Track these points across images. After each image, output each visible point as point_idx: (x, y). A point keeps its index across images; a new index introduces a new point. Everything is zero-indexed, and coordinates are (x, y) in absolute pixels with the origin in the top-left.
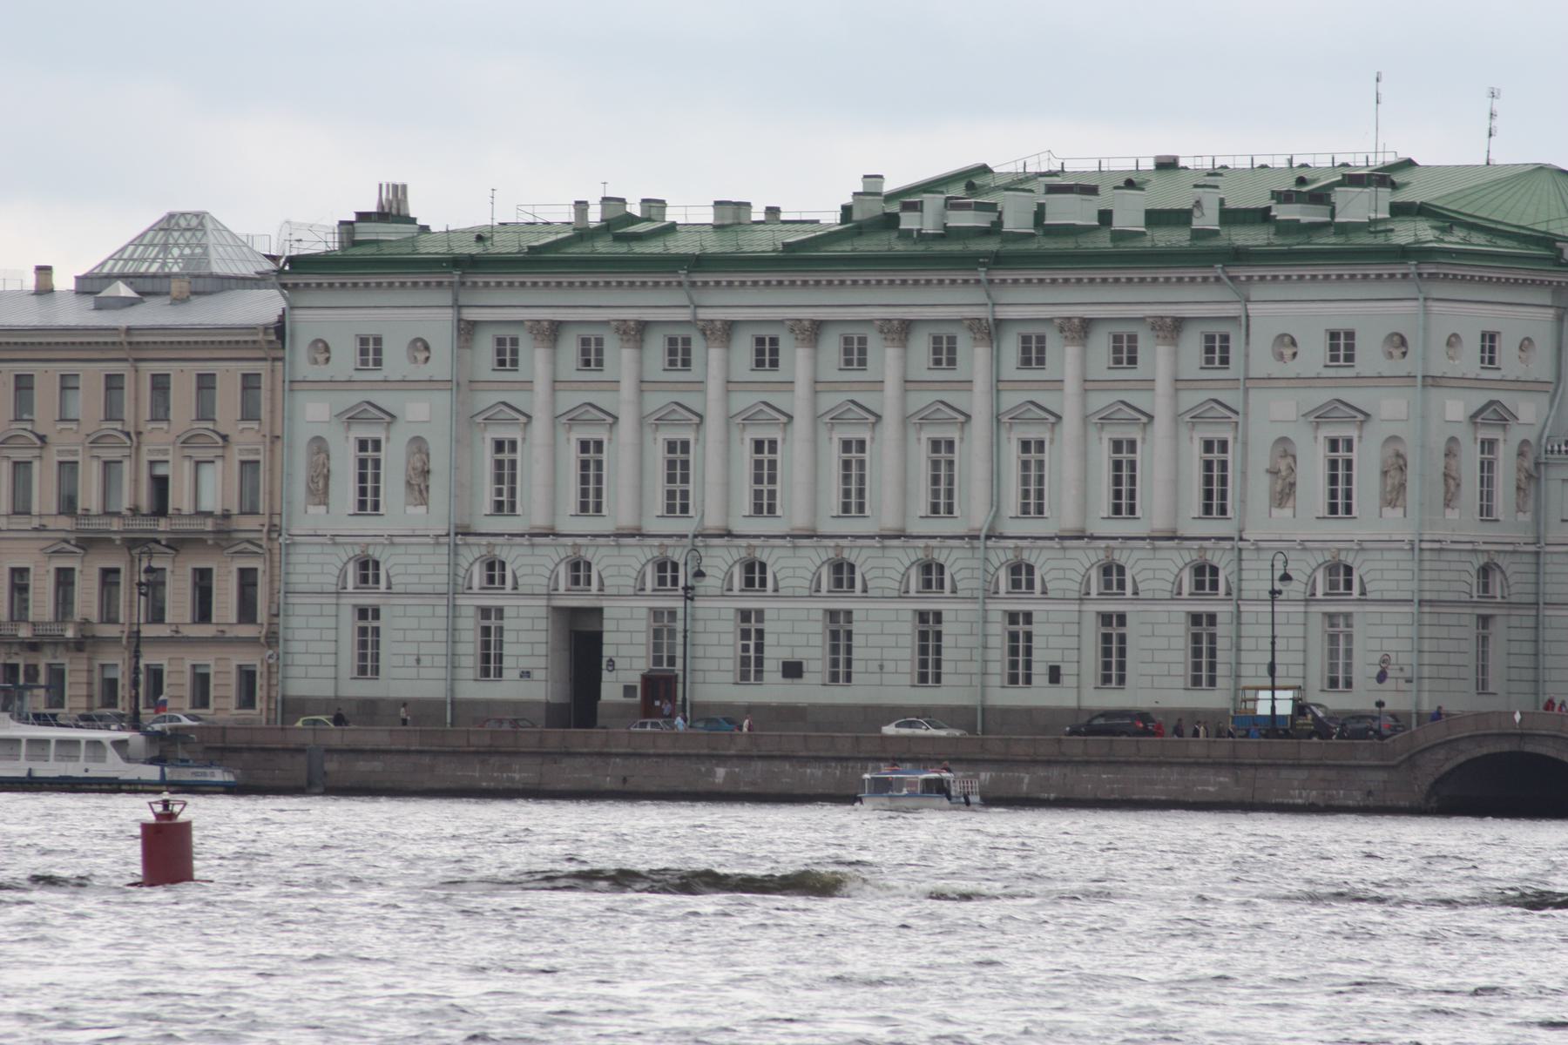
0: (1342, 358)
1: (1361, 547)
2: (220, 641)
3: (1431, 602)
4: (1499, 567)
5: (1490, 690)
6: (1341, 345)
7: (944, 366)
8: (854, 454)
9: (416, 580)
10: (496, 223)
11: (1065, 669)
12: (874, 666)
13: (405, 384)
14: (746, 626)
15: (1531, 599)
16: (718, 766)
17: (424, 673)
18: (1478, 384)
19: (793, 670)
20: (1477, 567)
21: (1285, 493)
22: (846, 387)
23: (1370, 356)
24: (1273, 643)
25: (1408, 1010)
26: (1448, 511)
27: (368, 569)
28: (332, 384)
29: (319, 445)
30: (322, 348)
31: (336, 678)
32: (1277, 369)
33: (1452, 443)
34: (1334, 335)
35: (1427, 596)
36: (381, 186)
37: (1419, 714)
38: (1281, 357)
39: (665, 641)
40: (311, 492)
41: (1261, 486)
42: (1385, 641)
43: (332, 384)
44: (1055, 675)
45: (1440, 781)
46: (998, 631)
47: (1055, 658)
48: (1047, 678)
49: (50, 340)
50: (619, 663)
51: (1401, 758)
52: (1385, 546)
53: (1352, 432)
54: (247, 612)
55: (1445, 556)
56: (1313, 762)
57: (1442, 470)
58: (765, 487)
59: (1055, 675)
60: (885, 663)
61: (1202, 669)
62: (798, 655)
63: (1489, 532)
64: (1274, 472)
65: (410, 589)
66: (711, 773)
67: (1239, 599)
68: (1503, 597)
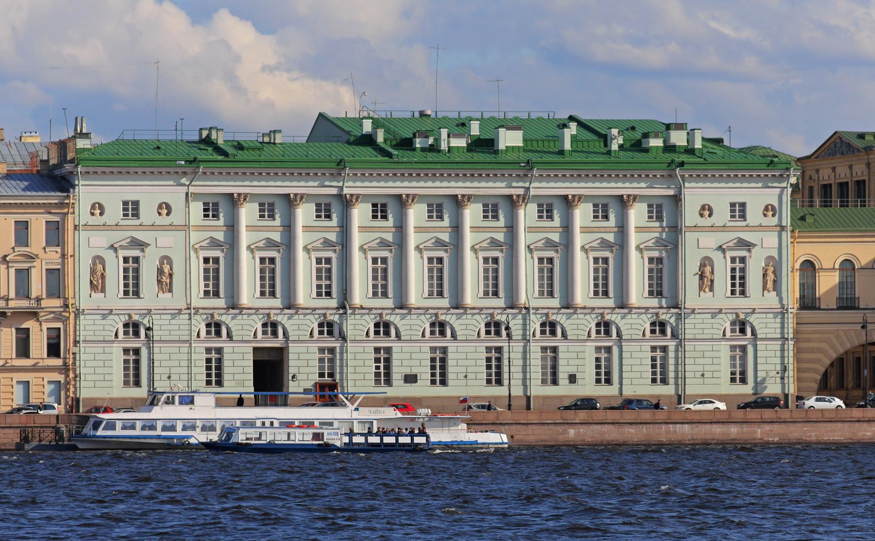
0: (130, 215)
2: (35, 369)
6: (132, 209)
7: (130, 217)
8: (323, 265)
9: (92, 333)
10: (70, 136)
12: (165, 377)
13: (153, 227)
14: (378, 356)
15: (187, 338)
16: (569, 428)
17: (470, 383)
19: (411, 379)
22: (431, 230)
23: (148, 214)
24: (509, 361)
27: (741, 326)
28: (104, 227)
29: (706, 262)
30: (706, 210)
32: (93, 220)
36: (76, 119)
38: (702, 215)
40: (93, 286)
41: (692, 282)
43: (104, 227)
44: (572, 379)
46: (200, 358)
47: (572, 370)
48: (568, 381)
49: (18, 202)
50: (299, 377)
52: (766, 311)
53: (135, 253)
54: (54, 350)
58: (324, 283)
59: (572, 379)
60: (468, 374)
61: (660, 376)
62: (414, 371)
65: (769, 336)
66: (565, 432)
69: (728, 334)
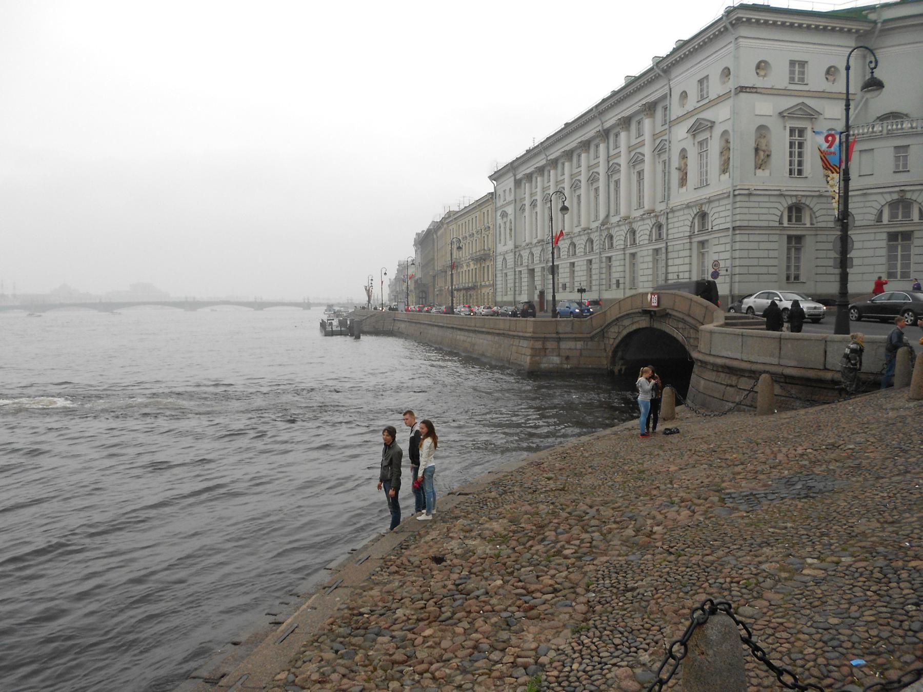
1: (710, 201)
3: (740, 228)
4: (808, 206)
5: (801, 281)
11: (568, 285)
18: (786, 92)
20: (786, 205)
21: (683, 181)
25: (211, 431)
26: (759, 172)
31: (690, 271)
33: (762, 130)
34: (792, 63)
35: (738, 224)
37: (733, 297)
39: (899, 253)
42: (766, 256)
45: (615, 352)
51: (597, 331)
55: (752, 198)
56: (459, 327)
57: (753, 145)
63: (902, 178)
64: (679, 169)
67: (667, 239)
68: (811, 224)
69: (786, 224)
